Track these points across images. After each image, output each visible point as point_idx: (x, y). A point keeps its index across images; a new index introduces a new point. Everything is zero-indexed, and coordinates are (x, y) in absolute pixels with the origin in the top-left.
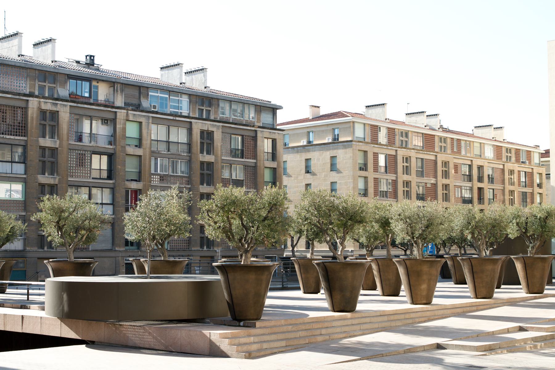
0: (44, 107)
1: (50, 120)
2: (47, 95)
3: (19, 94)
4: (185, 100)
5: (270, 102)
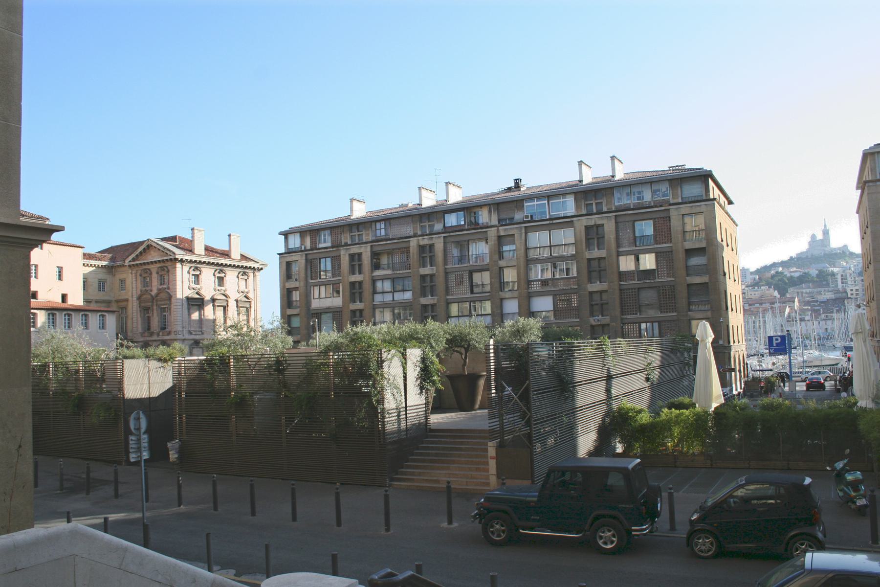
0: (422, 243)
1: (426, 252)
2: (595, 211)
3: (401, 238)
4: (570, 201)
5: (407, 206)
